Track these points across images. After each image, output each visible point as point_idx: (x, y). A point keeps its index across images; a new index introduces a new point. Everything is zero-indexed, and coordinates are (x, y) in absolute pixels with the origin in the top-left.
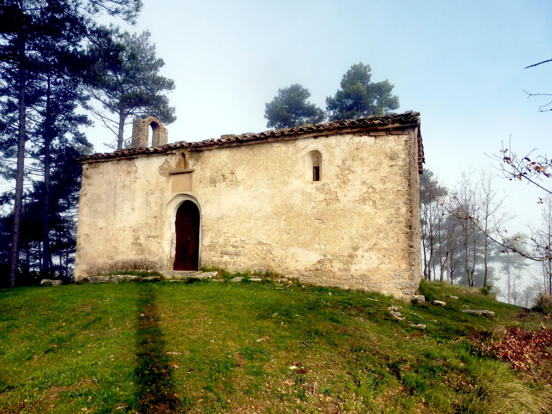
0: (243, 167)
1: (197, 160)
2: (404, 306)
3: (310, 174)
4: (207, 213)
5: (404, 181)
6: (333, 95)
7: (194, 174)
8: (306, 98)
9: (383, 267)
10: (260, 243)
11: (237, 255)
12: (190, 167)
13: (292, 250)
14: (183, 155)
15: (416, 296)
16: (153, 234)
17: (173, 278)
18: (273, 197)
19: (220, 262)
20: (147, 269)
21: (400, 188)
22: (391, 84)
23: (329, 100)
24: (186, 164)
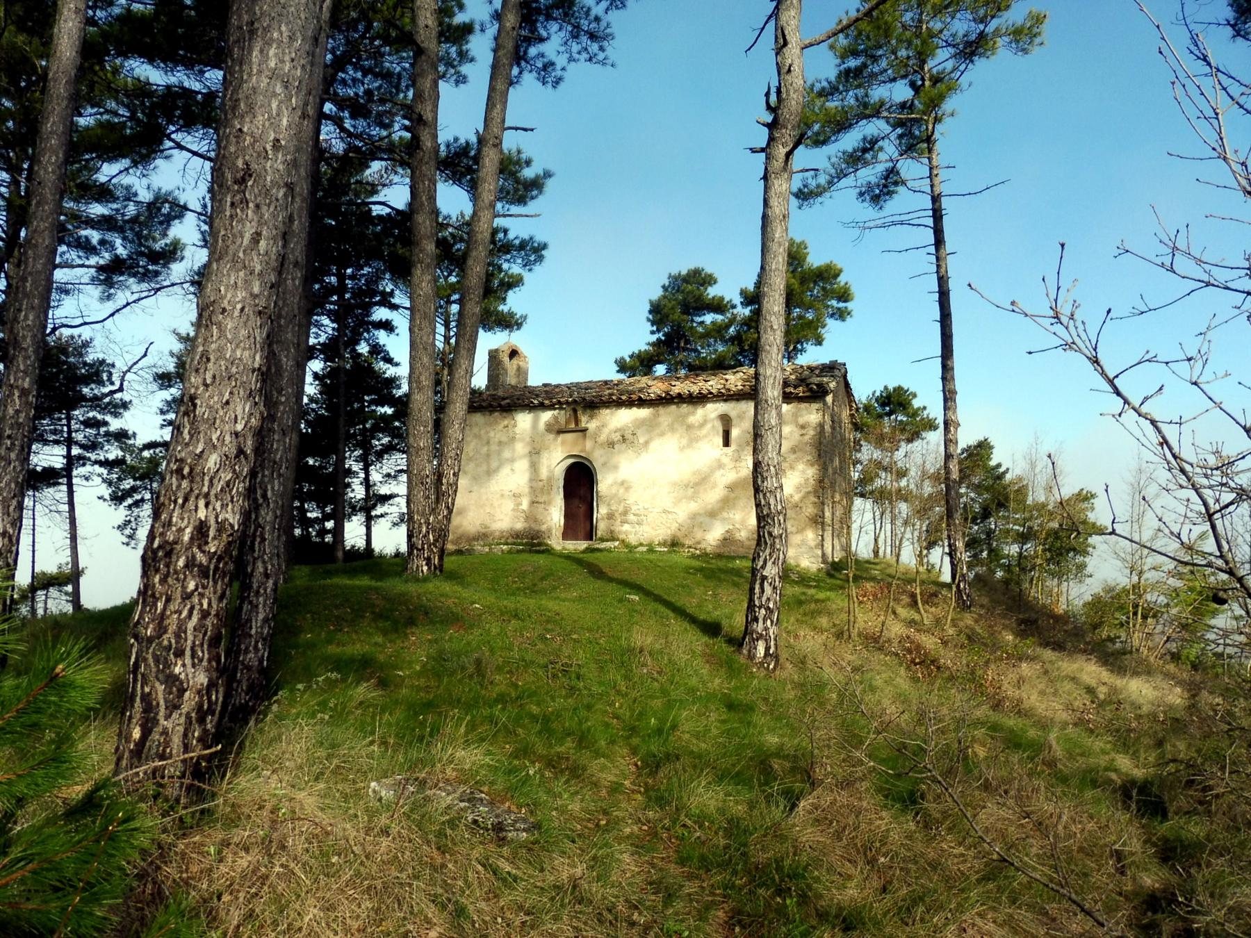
1: (592, 417)
2: (500, 406)
3: (720, 440)
10: (665, 511)
12: (583, 425)
14: (575, 411)
17: (564, 548)
22: (839, 266)
23: (743, 293)
24: (577, 422)
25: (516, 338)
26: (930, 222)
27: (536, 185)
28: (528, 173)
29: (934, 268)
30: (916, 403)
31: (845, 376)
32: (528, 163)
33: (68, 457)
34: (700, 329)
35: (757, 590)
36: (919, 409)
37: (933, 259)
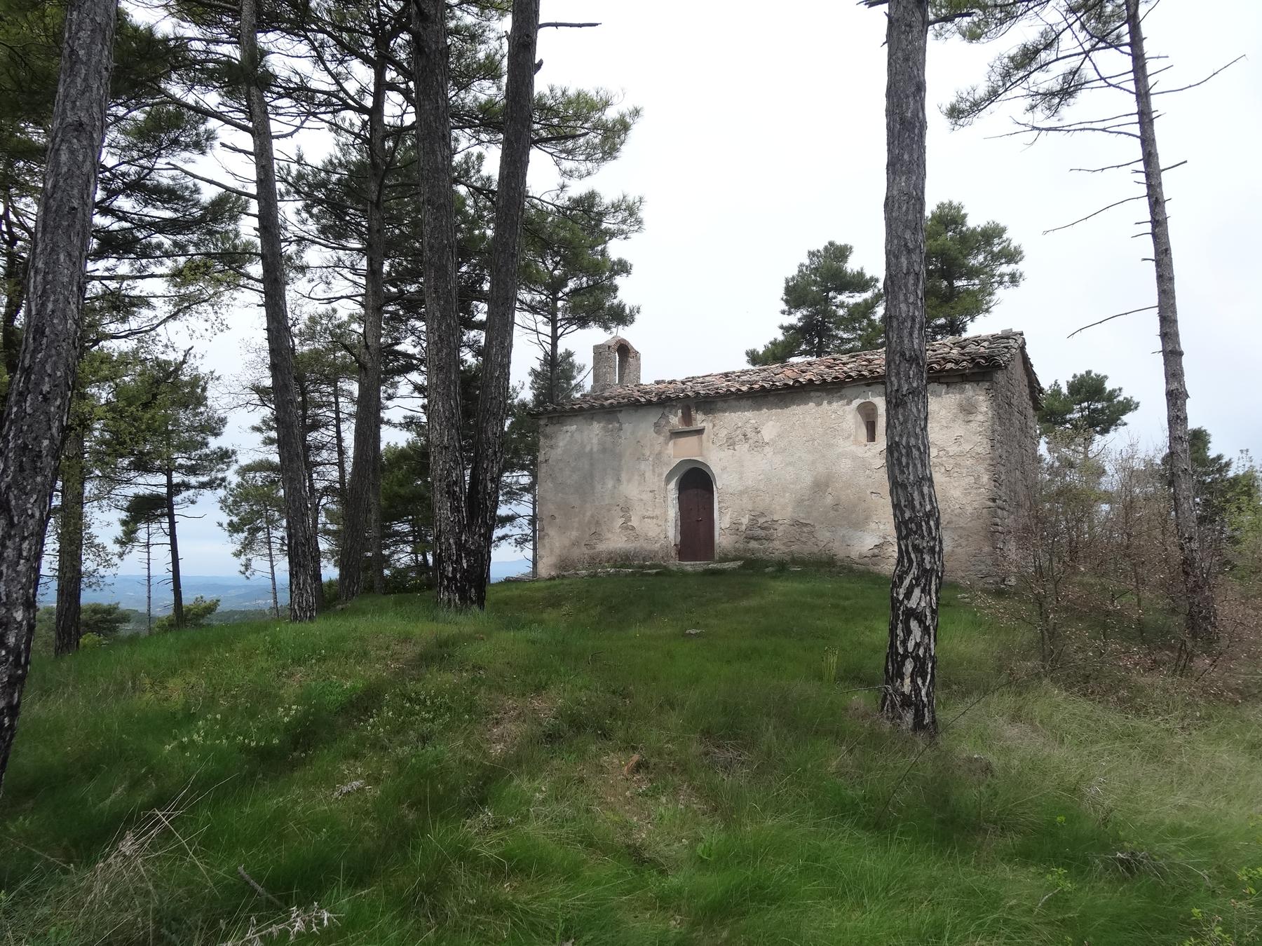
0: (771, 423)
4: (724, 482)
5: (985, 441)
6: (602, 330)
7: (704, 436)
8: (791, 327)
9: (959, 550)
11: (768, 539)
13: (842, 532)
15: (1149, 680)
16: (649, 513)
18: (813, 462)
19: (745, 550)
20: (644, 560)
21: (979, 450)
25: (623, 333)
26: (1136, 130)
27: (623, 126)
28: (611, 114)
29: (1143, 190)
30: (1109, 386)
31: (1022, 348)
32: (607, 104)
33: (169, 484)
34: (841, 312)
35: (900, 632)
36: (1114, 391)
37: (1142, 177)
